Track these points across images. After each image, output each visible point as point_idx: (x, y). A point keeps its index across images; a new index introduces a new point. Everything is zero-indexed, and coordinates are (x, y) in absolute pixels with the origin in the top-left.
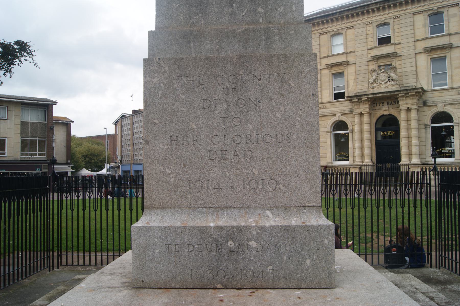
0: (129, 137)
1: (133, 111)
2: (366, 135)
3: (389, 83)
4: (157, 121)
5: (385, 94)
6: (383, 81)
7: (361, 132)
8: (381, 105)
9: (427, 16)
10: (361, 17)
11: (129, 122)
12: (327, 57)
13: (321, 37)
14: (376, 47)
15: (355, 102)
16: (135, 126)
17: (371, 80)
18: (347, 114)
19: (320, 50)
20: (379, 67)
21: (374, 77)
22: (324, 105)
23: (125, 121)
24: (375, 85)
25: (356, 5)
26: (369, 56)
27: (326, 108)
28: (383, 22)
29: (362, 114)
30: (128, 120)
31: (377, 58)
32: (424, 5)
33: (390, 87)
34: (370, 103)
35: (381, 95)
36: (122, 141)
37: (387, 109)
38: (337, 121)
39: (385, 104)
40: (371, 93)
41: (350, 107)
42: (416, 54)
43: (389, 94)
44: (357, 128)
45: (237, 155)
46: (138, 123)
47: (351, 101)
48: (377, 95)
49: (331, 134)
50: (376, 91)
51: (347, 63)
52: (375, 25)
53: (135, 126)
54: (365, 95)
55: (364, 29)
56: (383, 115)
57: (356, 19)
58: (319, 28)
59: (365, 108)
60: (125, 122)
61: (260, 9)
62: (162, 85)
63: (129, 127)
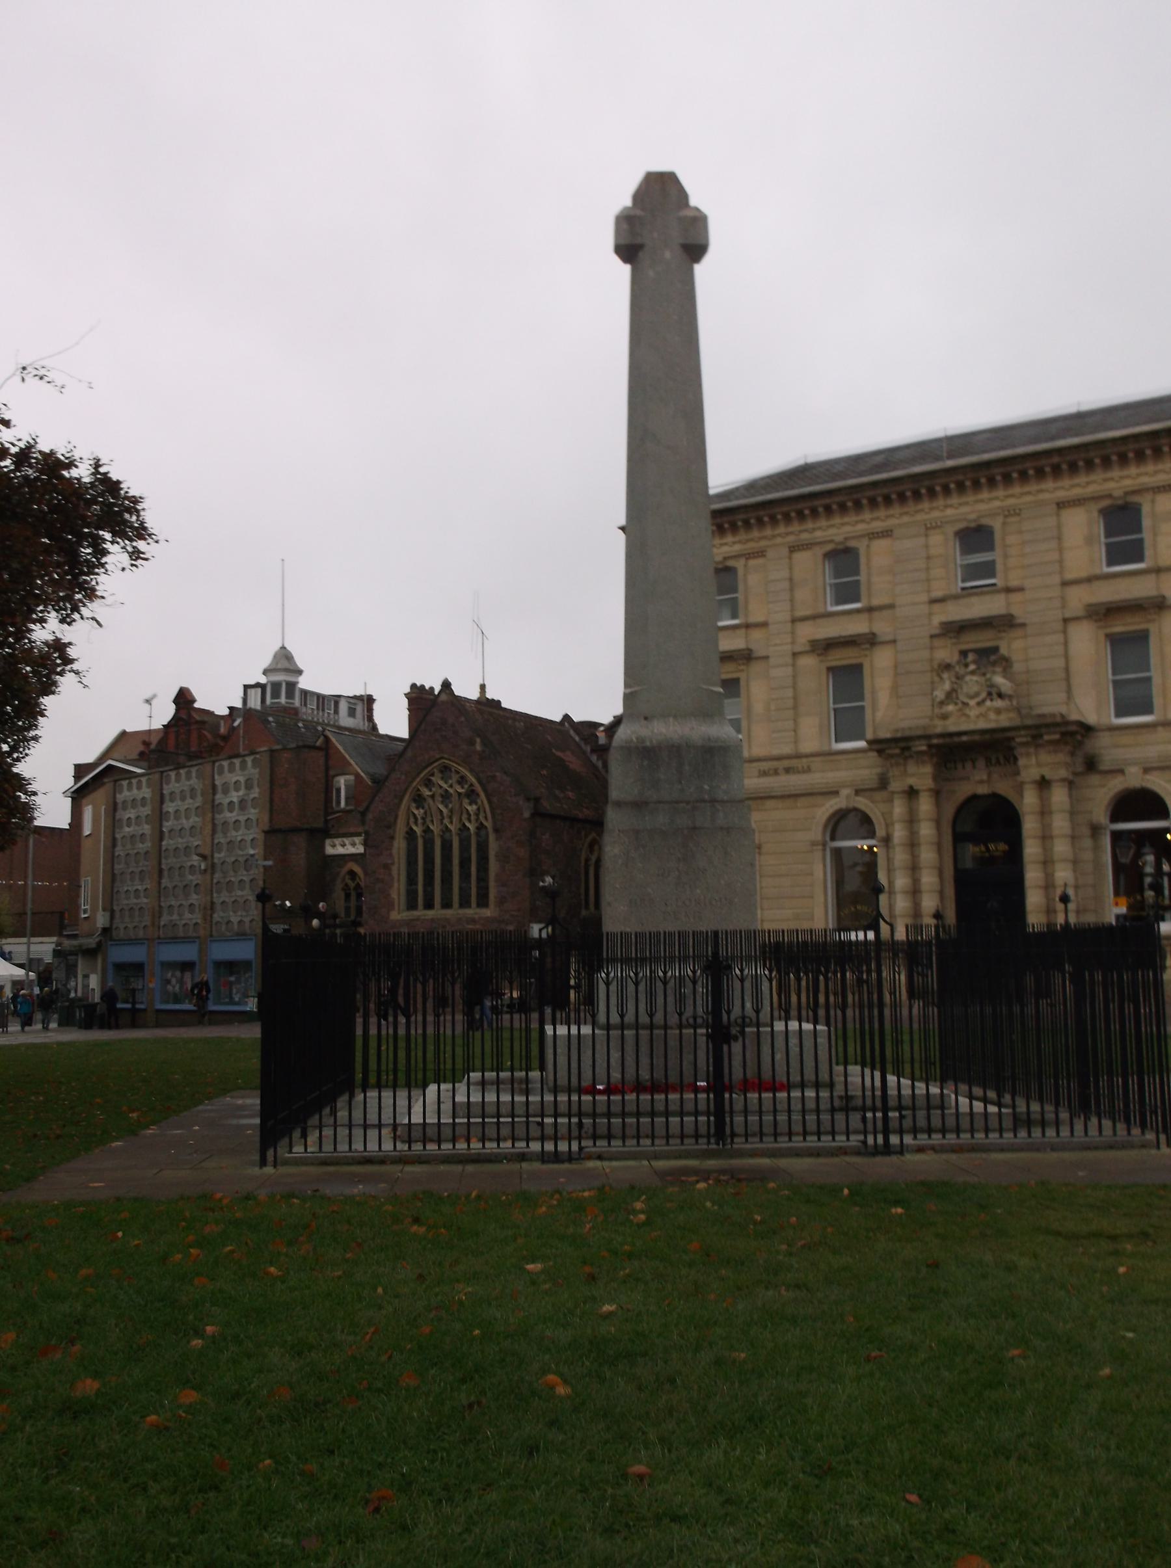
0: (142, 847)
1: (566, 717)
2: (927, 855)
3: (988, 703)
5: (977, 737)
6: (972, 697)
7: (912, 844)
8: (969, 765)
9: (951, 536)
10: (911, 507)
11: (146, 792)
12: (814, 617)
14: (956, 597)
15: (892, 756)
16: (170, 807)
17: (940, 694)
18: (871, 790)
20: (964, 653)
21: (947, 686)
22: (804, 760)
24: (950, 708)
25: (914, 461)
26: (937, 620)
27: (808, 770)
28: (973, 525)
29: (912, 793)
31: (956, 629)
33: (992, 716)
34: (935, 760)
35: (964, 738)
36: (111, 859)
37: (985, 777)
39: (981, 763)
40: (939, 730)
41: (879, 770)
43: (987, 737)
44: (899, 833)
46: (183, 799)
47: (880, 752)
48: (956, 739)
49: (824, 850)
50: (952, 726)
51: (870, 641)
52: (951, 530)
53: (170, 810)
54: (919, 737)
55: (922, 540)
56: (974, 798)
57: (896, 510)
59: (921, 775)
60: (126, 793)
61: (706, 787)
63: (146, 811)
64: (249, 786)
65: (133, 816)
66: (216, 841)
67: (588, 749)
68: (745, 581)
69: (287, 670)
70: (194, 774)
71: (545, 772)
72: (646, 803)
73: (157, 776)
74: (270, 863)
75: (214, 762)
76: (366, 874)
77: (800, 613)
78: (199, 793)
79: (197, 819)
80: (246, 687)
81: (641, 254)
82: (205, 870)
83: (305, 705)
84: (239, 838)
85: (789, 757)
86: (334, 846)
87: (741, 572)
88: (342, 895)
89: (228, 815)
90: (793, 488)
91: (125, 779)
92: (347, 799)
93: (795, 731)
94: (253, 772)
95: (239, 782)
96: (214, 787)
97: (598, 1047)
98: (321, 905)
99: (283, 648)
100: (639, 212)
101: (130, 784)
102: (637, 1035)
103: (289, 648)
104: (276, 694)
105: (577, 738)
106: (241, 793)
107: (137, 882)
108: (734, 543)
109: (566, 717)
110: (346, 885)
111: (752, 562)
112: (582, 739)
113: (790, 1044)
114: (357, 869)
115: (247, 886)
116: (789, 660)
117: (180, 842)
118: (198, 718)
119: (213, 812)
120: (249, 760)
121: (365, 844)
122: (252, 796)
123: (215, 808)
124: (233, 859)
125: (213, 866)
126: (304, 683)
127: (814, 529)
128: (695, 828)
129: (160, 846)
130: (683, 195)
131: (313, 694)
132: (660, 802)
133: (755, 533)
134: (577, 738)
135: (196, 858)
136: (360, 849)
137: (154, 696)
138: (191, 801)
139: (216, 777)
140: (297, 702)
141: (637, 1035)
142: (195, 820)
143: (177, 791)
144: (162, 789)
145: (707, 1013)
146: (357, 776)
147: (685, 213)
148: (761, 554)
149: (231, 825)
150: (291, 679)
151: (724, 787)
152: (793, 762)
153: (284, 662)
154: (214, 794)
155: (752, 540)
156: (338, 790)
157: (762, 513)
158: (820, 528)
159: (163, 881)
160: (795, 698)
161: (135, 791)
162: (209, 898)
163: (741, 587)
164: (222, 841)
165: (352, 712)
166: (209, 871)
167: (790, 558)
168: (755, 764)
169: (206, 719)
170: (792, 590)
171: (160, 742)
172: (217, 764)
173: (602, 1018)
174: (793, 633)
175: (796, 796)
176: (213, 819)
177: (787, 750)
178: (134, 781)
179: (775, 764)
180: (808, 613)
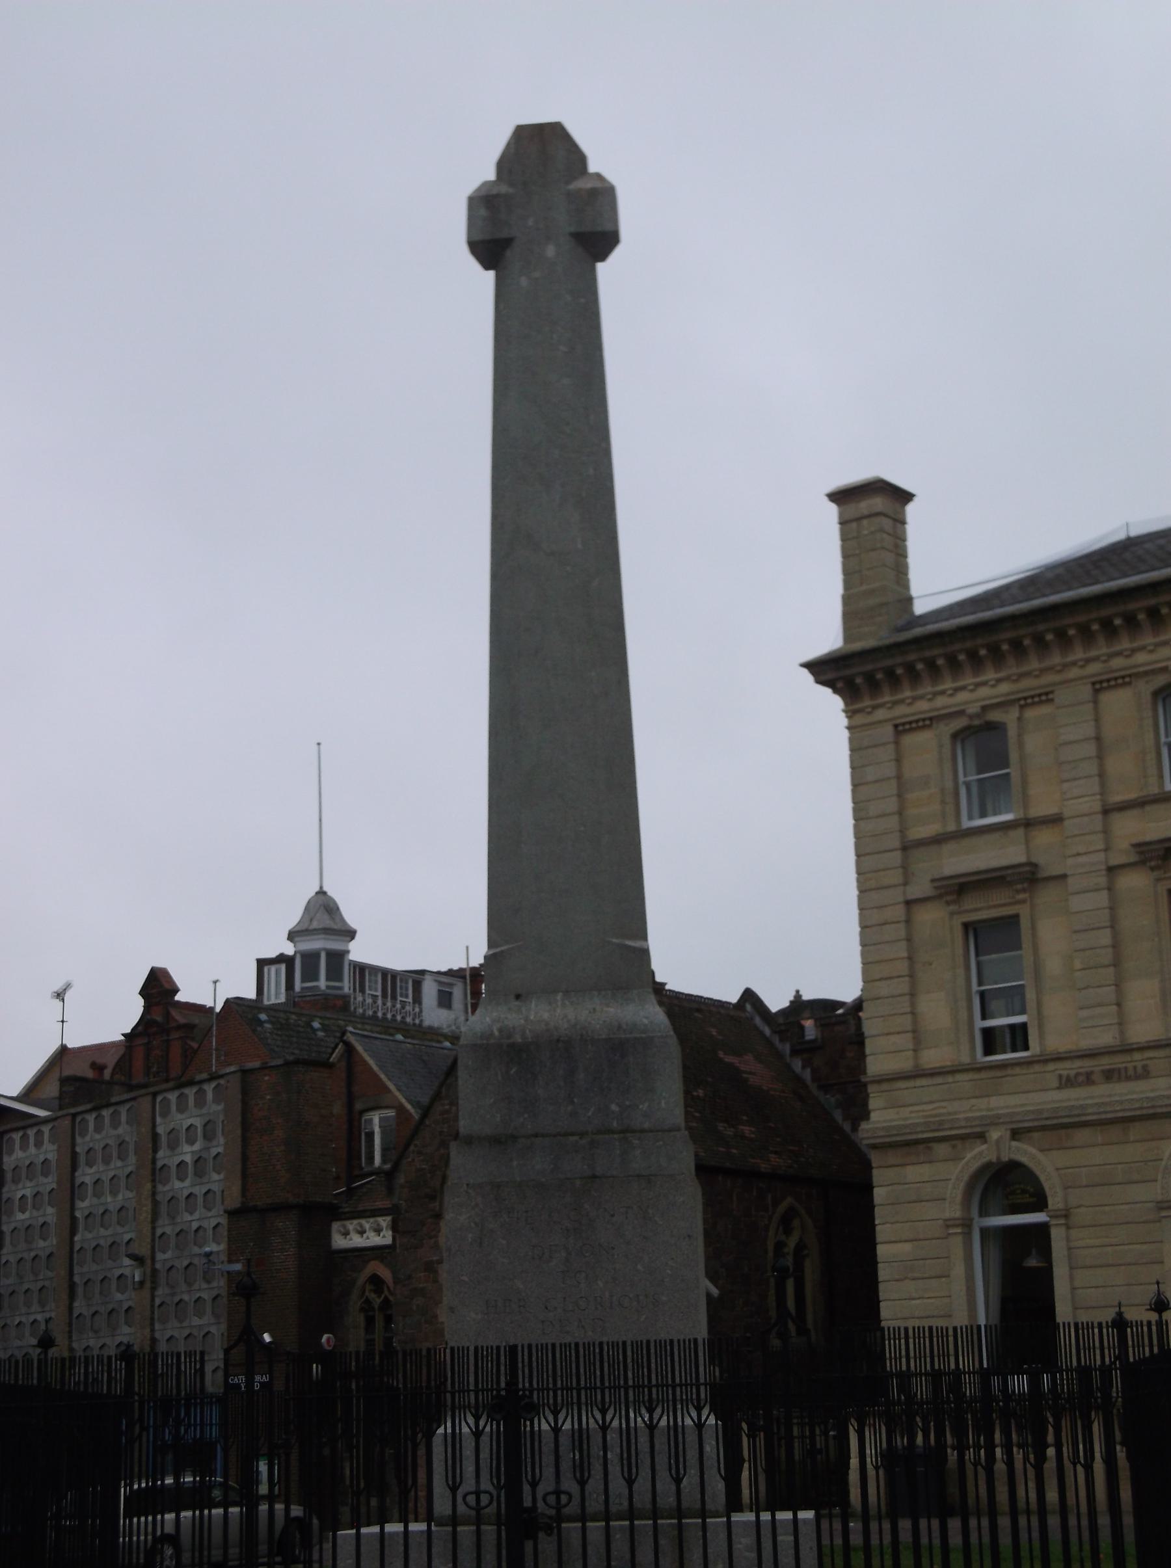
0: (43, 1246)
1: (749, 996)
4: (465, 1278)
11: (50, 1151)
12: (1140, 804)
13: (1106, 698)
16: (86, 1175)
19: (1101, 766)
22: (1137, 1056)
23: (24, 1146)
27: (1144, 1074)
30: (39, 1144)
32: (1157, 645)
38: (988, 1166)
42: (909, 903)
45: (583, 1327)
46: (107, 1161)
49: (968, 1235)
53: (88, 1180)
58: (1093, 653)
60: (19, 1154)
61: (614, 1107)
62: (473, 1225)
63: (49, 1183)
64: (209, 1136)
65: (28, 1192)
66: (159, 1232)
67: (786, 1048)
68: (1021, 745)
69: (327, 931)
70: (124, 1118)
71: (701, 1093)
72: (514, 1138)
73: (67, 1122)
74: (238, 1267)
75: (155, 1095)
76: (396, 1281)
77: (1117, 798)
78: (131, 1147)
79: (130, 1195)
80: (262, 963)
81: (508, 253)
82: (142, 1283)
83: (362, 990)
84: (195, 1225)
85: (1109, 1052)
86: (346, 1234)
87: (1012, 732)
88: (361, 1319)
89: (178, 1184)
90: (1097, 582)
91: (17, 1129)
92: (384, 1150)
93: (1119, 1005)
94: (215, 1108)
95: (194, 1124)
96: (155, 1137)
97: (413, 1555)
98: (325, 1337)
99: (321, 893)
100: (504, 189)
101: (25, 1138)
102: (478, 1532)
103: (331, 892)
104: (310, 973)
105: (767, 1031)
106: (197, 1147)
107: (35, 1307)
108: (999, 681)
109: (749, 996)
110: (367, 1301)
111: (1030, 713)
112: (774, 1032)
113: (736, 1546)
114: (385, 1274)
115: (209, 1309)
116: (1102, 881)
117: (104, 1235)
118: (182, 1020)
119: (153, 1181)
120: (209, 1088)
121: (394, 1228)
122: (214, 1151)
123: (157, 1174)
124: (186, 1263)
125: (155, 1272)
126: (358, 952)
127: (1134, 651)
128: (594, 1177)
129: (72, 1243)
130: (577, 158)
131: (374, 970)
132: (536, 1136)
133: (1034, 664)
134: (767, 1031)
135: (127, 1261)
136: (386, 1238)
137: (68, 986)
138: (119, 1163)
139: (159, 1120)
140: (346, 986)
141: (478, 1532)
142: (124, 1196)
143: (99, 1146)
144: (73, 1145)
145: (498, 1487)
146: (400, 1109)
147: (582, 184)
148: (1044, 697)
149: (183, 1204)
150: (335, 945)
151: (644, 1107)
152: (1118, 1060)
153: (324, 918)
154: (155, 1150)
155: (1050, 669)
156: (370, 1136)
157: (1041, 627)
158: (1142, 648)
159: (76, 1304)
160: (1115, 946)
161: (32, 1150)
162: (147, 1331)
163: (1014, 756)
164: (168, 1230)
165: (445, 1000)
166: (148, 1285)
167: (1096, 702)
168: (1051, 1067)
169: (195, 1020)
170: (1100, 757)
171: (119, 1066)
172: (159, 1098)
173: (442, 1506)
174: (1106, 831)
175: (1127, 1121)
176: (154, 1194)
177: (1107, 1038)
178: (31, 1133)
179: (1087, 1064)
180: (1133, 796)
